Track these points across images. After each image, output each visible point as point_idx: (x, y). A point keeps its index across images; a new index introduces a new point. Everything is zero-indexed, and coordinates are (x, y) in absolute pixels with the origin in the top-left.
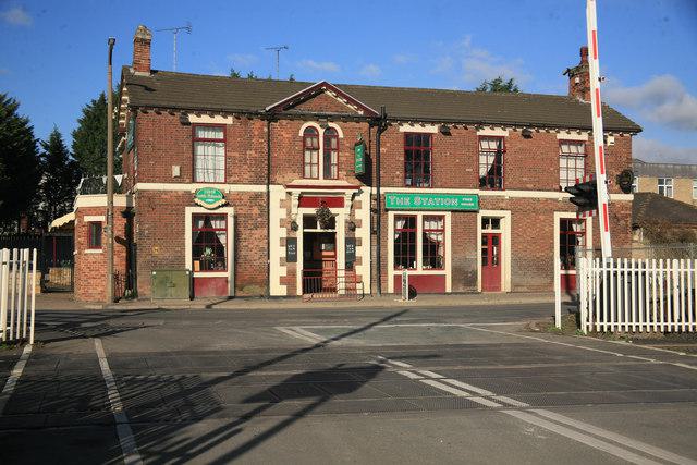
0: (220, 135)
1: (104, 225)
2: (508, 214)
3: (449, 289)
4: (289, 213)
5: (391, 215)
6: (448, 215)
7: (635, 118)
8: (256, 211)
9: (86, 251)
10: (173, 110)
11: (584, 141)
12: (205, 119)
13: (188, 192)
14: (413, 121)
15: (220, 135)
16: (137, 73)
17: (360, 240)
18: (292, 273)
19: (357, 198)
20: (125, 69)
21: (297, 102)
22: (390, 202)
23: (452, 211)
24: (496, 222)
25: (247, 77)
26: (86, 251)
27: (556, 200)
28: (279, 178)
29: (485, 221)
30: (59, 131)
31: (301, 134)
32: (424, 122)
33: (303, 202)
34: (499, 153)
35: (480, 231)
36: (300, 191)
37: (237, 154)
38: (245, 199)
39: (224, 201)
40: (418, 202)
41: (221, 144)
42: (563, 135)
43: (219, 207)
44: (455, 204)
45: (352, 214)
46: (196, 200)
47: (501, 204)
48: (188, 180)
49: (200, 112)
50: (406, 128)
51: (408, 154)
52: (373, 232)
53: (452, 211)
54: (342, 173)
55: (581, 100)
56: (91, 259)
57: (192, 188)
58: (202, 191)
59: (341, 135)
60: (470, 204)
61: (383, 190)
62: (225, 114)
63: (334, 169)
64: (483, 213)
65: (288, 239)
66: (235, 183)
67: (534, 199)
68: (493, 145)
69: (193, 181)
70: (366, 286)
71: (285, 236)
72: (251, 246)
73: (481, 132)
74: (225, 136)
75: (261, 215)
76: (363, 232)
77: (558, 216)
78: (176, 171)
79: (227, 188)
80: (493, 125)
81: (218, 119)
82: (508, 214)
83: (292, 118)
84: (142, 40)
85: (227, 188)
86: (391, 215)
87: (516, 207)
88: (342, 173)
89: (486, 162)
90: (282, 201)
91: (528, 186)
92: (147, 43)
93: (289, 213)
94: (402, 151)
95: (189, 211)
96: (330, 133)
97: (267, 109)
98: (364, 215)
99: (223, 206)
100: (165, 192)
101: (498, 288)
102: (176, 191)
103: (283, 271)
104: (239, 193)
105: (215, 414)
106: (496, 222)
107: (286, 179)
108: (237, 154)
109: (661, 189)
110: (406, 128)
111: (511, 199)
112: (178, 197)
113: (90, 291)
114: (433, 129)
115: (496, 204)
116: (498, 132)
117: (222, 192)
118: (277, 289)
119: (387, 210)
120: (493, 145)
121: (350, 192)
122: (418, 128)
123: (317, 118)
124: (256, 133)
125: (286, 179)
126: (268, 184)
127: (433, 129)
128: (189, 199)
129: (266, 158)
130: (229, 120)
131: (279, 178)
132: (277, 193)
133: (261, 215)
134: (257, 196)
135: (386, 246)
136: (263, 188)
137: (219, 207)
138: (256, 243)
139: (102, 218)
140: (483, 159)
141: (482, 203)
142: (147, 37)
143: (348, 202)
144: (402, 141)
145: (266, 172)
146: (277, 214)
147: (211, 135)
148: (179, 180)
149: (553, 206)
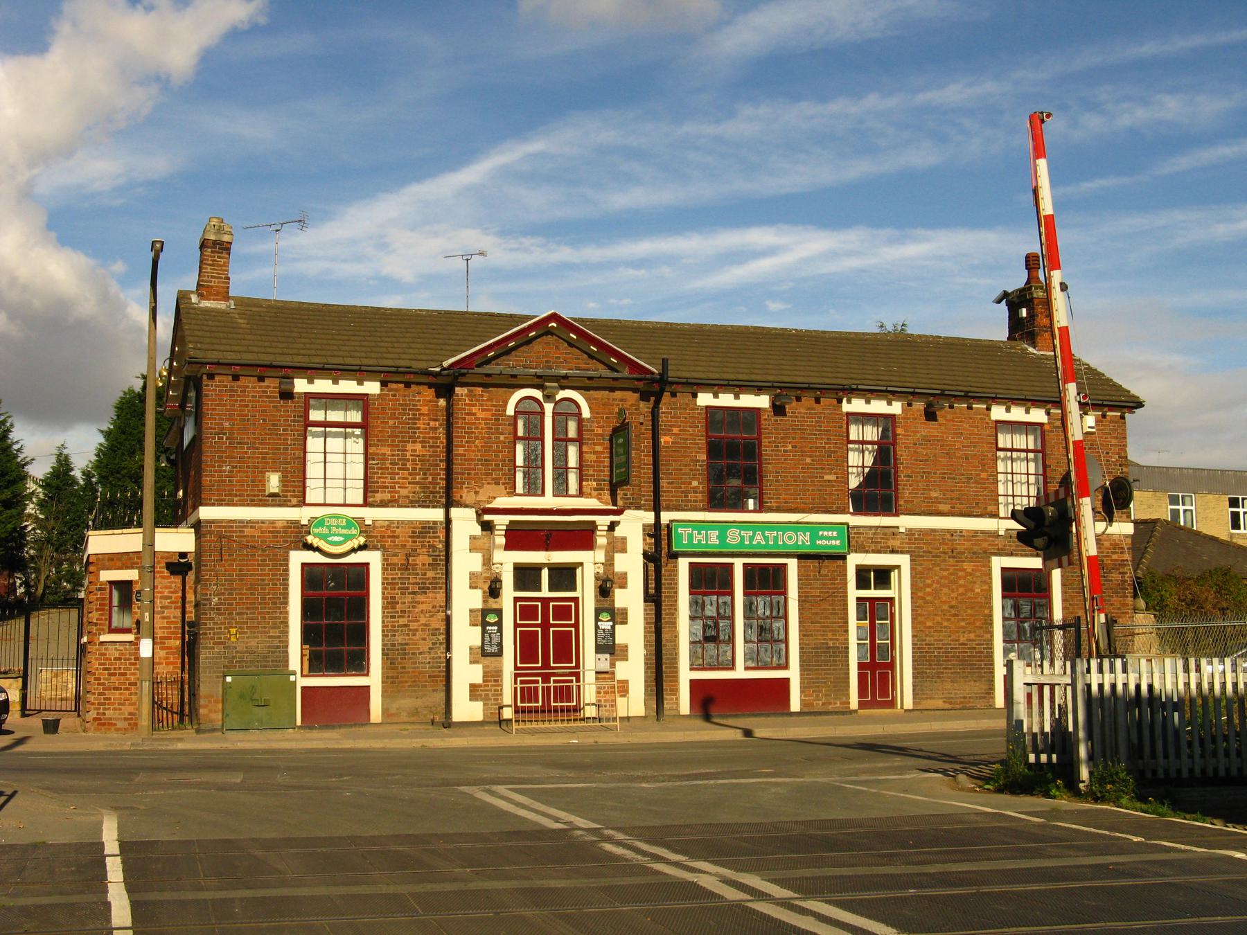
0: (355, 416)
1: (136, 588)
2: (903, 561)
3: (795, 705)
4: (488, 562)
5: (683, 564)
6: (792, 565)
7: (1136, 388)
8: (423, 559)
9: (105, 638)
10: (262, 370)
11: (1041, 425)
12: (323, 385)
13: (295, 524)
14: (718, 387)
15: (355, 416)
16: (206, 304)
17: (625, 648)
18: (493, 677)
19: (619, 532)
20: (182, 298)
21: (503, 350)
22: (683, 539)
23: (801, 557)
24: (883, 576)
25: (894, 403)
26: (103, 638)
27: (994, 534)
28: (467, 495)
29: (862, 573)
30: (998, 293)
31: (510, 411)
32: (738, 387)
33: (518, 538)
34: (885, 451)
35: (853, 593)
36: (506, 519)
37: (387, 451)
38: (403, 535)
39: (362, 540)
40: (734, 538)
41: (358, 431)
42: (998, 413)
43: (354, 550)
44: (803, 541)
45: (609, 562)
46: (310, 539)
47: (891, 543)
48: (294, 501)
49: (312, 372)
50: (705, 399)
51: (713, 450)
52: (647, 598)
53: (801, 557)
54: (590, 485)
55: (1031, 349)
56: (113, 653)
57: (302, 515)
58: (319, 522)
59: (586, 413)
60: (831, 542)
61: (666, 517)
62: (360, 373)
63: (573, 479)
64: (854, 560)
65: (485, 612)
66: (383, 504)
67: (952, 533)
68: (871, 433)
69: (303, 503)
70: (635, 703)
71: (479, 605)
72: (413, 626)
73: (846, 407)
74: (365, 416)
75: (433, 566)
76: (631, 598)
77: (998, 563)
78: (274, 482)
79: (372, 515)
80: (869, 394)
81: (348, 386)
82: (903, 561)
83: (488, 383)
84: (215, 243)
85: (372, 515)
86: (683, 564)
87: (917, 545)
88: (590, 485)
89: (859, 462)
90: (473, 538)
91: (943, 507)
92: (225, 248)
93: (488, 562)
94: (702, 441)
95: (298, 558)
96: (566, 412)
97: (445, 364)
98: (631, 564)
99: (362, 548)
100: (252, 523)
101: (891, 704)
102: (272, 522)
103: (476, 674)
104: (390, 524)
105: (583, 391)
106: (883, 576)
107: (481, 497)
108: (387, 451)
109: (1175, 513)
110: (705, 399)
111: (911, 532)
112: (274, 532)
113: (109, 714)
114: (762, 401)
115: (882, 541)
116: (878, 406)
117: (360, 521)
118: (465, 709)
119: (675, 556)
120: (871, 433)
121: (603, 521)
122: (726, 400)
123: (538, 382)
124: (425, 410)
125: (481, 497)
126: (449, 504)
127: (762, 401)
128: (297, 536)
129: (443, 456)
130: (372, 388)
131: (467, 495)
132: (464, 523)
133: (433, 566)
134: (426, 528)
135: (674, 624)
136: (437, 514)
137: (354, 550)
138: (423, 620)
139: (131, 575)
140: (854, 458)
141: (855, 540)
142: (226, 238)
143: (601, 540)
144: (701, 426)
145: (443, 484)
146: (465, 563)
147: (335, 416)
148: (275, 500)
149: (988, 544)
